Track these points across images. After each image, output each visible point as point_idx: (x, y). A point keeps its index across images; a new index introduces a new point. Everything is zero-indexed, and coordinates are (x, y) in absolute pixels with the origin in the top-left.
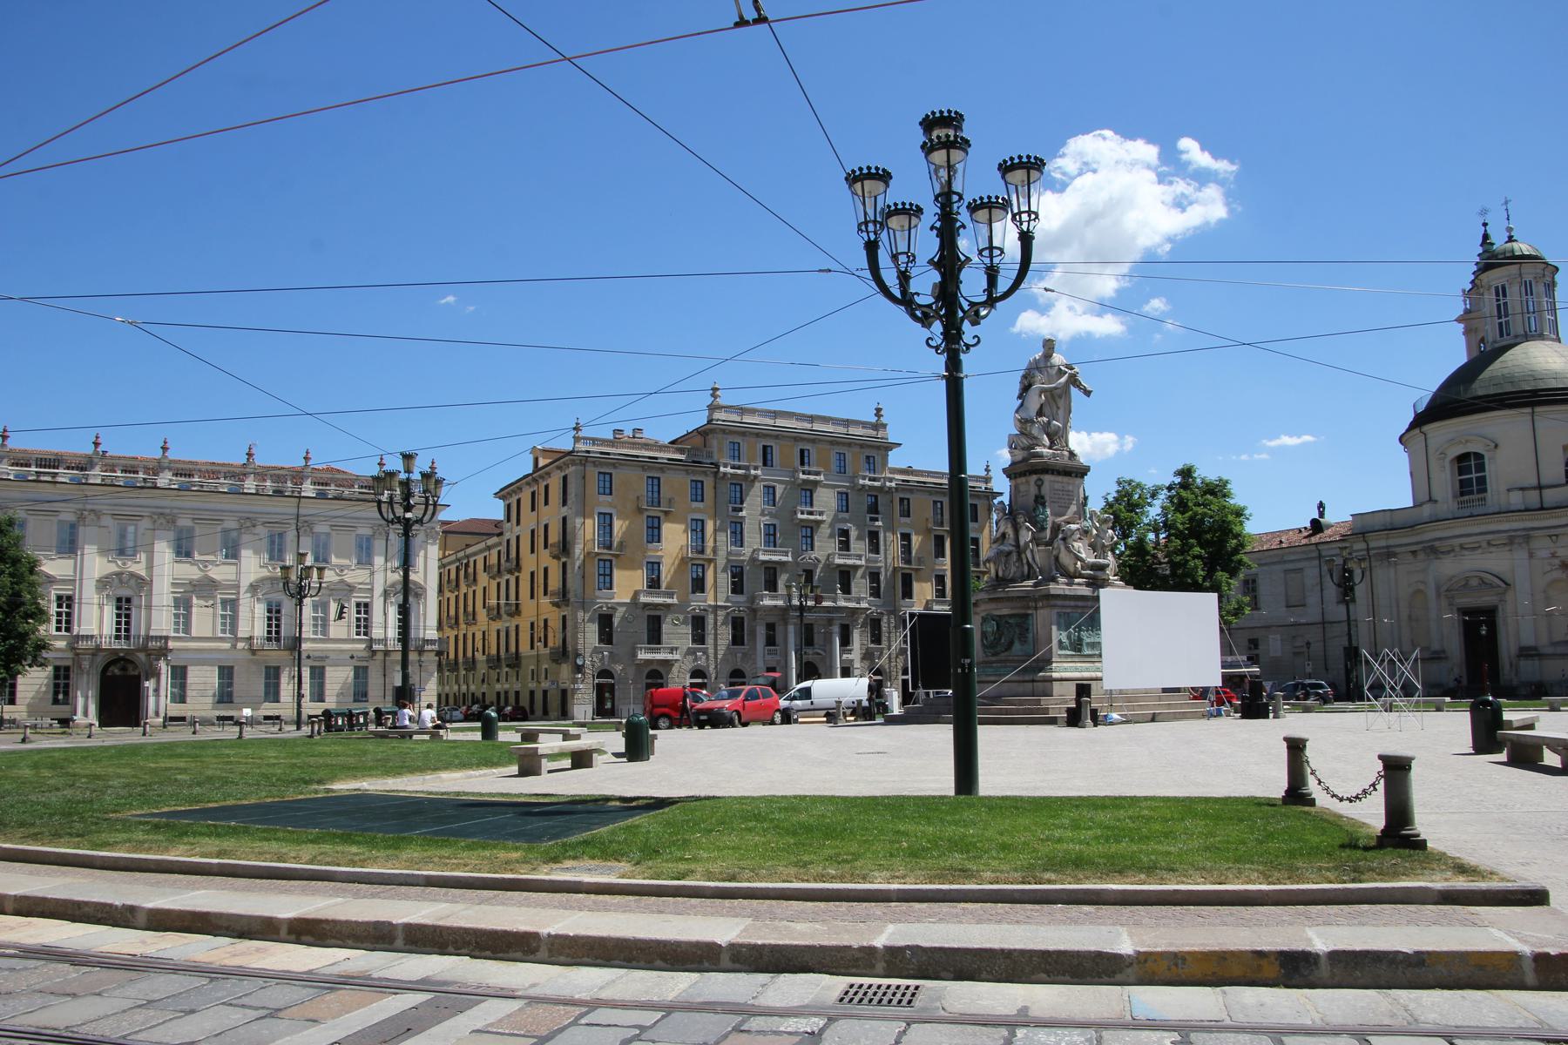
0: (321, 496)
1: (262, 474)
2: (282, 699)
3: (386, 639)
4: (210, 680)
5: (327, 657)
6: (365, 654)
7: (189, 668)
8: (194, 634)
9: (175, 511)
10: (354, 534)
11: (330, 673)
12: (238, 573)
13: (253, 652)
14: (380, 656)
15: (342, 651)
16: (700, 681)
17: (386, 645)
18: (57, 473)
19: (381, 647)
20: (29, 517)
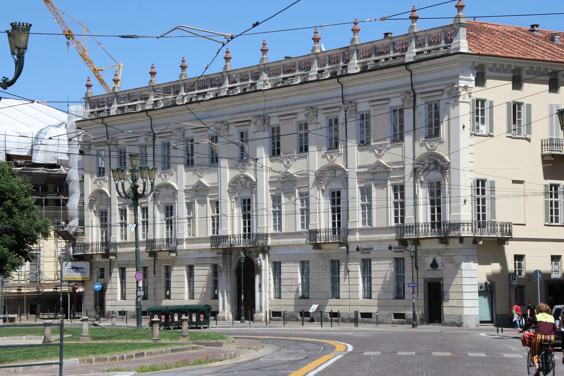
0: (364, 70)
1: (272, 70)
2: (342, 295)
3: (417, 225)
4: (294, 276)
5: (371, 249)
6: (396, 244)
7: (127, 270)
8: (375, 225)
9: (267, 111)
10: (295, 121)
11: (375, 266)
12: (308, 166)
13: (317, 246)
14: (411, 248)
15: (381, 241)
16: (517, 266)
17: (417, 233)
18: (206, 93)
19: (413, 236)
20: (281, 123)
